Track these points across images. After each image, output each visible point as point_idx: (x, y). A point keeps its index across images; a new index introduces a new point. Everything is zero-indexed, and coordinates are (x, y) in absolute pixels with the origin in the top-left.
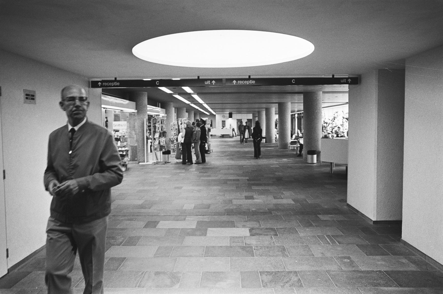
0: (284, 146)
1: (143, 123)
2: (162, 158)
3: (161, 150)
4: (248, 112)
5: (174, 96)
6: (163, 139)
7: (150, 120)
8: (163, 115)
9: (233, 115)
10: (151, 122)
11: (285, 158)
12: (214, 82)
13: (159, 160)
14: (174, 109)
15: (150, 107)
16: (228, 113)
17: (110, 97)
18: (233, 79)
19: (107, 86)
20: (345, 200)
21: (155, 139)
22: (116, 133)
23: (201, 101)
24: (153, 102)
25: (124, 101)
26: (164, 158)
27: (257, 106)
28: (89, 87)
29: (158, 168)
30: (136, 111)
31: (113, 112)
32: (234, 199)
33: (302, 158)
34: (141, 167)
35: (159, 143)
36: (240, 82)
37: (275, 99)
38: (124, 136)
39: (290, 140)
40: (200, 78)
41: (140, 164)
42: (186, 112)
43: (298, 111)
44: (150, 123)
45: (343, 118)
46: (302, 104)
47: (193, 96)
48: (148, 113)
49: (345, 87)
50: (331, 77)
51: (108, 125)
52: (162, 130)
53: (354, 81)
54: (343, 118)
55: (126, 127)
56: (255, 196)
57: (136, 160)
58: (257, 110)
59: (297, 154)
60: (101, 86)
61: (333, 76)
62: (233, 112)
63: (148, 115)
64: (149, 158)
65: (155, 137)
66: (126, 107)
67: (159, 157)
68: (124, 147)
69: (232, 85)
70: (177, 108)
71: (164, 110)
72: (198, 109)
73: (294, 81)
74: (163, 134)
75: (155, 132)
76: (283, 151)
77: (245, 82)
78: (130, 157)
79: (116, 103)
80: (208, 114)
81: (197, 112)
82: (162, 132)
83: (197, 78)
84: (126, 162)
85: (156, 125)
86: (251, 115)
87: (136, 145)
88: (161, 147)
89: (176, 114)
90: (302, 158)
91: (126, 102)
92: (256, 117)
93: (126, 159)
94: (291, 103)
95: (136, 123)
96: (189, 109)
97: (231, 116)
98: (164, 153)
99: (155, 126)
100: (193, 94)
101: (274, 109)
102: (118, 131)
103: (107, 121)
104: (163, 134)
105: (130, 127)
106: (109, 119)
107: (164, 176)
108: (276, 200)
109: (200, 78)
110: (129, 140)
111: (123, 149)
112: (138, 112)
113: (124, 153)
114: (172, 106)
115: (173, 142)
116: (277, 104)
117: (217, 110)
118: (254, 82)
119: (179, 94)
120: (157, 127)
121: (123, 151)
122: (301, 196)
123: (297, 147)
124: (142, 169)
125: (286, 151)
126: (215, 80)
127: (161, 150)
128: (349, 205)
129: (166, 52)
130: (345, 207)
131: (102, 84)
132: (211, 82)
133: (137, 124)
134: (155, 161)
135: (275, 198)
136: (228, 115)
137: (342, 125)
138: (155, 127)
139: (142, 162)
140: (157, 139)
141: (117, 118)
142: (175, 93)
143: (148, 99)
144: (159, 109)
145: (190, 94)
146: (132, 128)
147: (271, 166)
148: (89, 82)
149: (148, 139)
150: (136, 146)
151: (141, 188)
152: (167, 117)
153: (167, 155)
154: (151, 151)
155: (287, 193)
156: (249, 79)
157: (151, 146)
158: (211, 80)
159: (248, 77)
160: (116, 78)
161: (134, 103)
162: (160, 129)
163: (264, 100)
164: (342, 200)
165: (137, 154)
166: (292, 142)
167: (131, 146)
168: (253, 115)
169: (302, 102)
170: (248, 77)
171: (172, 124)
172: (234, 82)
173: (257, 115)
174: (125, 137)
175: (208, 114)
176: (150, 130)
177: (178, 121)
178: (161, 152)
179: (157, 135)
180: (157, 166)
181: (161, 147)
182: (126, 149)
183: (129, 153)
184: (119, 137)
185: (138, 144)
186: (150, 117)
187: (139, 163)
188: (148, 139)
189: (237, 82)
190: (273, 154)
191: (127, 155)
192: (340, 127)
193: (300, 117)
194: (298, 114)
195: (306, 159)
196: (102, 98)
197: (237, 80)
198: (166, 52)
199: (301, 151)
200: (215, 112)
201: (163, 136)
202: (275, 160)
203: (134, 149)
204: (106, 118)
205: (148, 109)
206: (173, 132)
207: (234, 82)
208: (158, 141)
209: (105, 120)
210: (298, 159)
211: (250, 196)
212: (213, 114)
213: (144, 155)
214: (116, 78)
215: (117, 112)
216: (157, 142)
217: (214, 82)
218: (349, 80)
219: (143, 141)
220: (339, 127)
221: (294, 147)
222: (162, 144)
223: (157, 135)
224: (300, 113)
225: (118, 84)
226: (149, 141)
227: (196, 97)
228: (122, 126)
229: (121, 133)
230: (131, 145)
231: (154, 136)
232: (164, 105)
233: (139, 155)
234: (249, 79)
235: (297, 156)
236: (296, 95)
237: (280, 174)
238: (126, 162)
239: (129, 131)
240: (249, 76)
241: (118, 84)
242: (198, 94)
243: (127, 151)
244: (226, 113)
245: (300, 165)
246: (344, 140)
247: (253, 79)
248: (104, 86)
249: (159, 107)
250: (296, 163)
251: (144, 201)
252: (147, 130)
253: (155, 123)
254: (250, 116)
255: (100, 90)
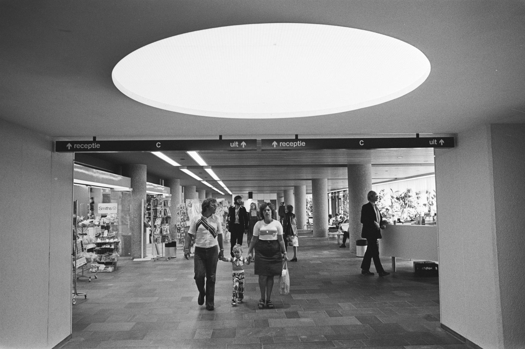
0: (321, 234)
1: (141, 206)
2: (164, 251)
3: (163, 241)
4: (272, 192)
5: (182, 170)
6: (166, 227)
7: (150, 202)
8: (167, 195)
9: (254, 195)
10: (151, 203)
11: (325, 250)
12: (243, 144)
13: (161, 255)
14: (181, 187)
15: (149, 185)
16: (248, 192)
17: (94, 170)
18: (273, 141)
19: (80, 150)
20: (437, 318)
21: (155, 226)
22: (103, 218)
23: (215, 177)
24: (154, 178)
25: (114, 177)
26: (168, 253)
27: (283, 183)
28: (53, 151)
29: (159, 267)
30: (131, 190)
31: (102, 191)
32: (271, 317)
33: (349, 250)
34: (136, 266)
35: (161, 232)
36: (284, 144)
37: (307, 174)
38: (112, 223)
39: (328, 225)
40: (223, 138)
41: (135, 260)
42: (196, 191)
43: (332, 190)
44: (149, 205)
45: (392, 197)
46: (347, 181)
47: (206, 170)
48: (147, 192)
49: (428, 154)
50: (415, 137)
51: (94, 208)
52: (165, 214)
53: (447, 143)
54: (392, 197)
55: (116, 211)
56: (300, 313)
57: (130, 256)
58: (283, 188)
59: (339, 244)
60: (72, 150)
61: (418, 135)
62: (253, 192)
63: (147, 195)
64: (147, 252)
65: (156, 224)
66: (119, 184)
67: (160, 251)
68: (113, 237)
69: (272, 148)
70: (185, 187)
71: (169, 189)
72: (211, 188)
73: (362, 143)
74: (166, 220)
75: (155, 217)
76: (319, 240)
77: (291, 144)
78: (120, 251)
79: (103, 178)
80: (223, 194)
81: (209, 191)
82: (165, 216)
83: (218, 139)
84: (114, 259)
85: (158, 208)
86: (276, 194)
87: (130, 234)
88: (164, 238)
89: (183, 194)
90: (349, 250)
91: (118, 178)
92: (281, 197)
93: (114, 255)
94: (328, 179)
95: (131, 206)
96: (200, 188)
97: (250, 196)
98: (167, 245)
99: (156, 209)
100: (207, 167)
101: (306, 188)
102: (106, 216)
103: (93, 203)
104: (166, 220)
105: (123, 211)
106: (95, 200)
107: (166, 280)
108: (334, 318)
109: (223, 138)
110: (120, 228)
111: (112, 241)
112: (133, 191)
113: (113, 247)
114: (179, 184)
115: (179, 230)
116: (311, 181)
117: (233, 189)
118: (303, 144)
119: (189, 168)
120: (158, 211)
121: (110, 244)
122: (368, 312)
123: (339, 236)
124: (137, 268)
125: (324, 240)
126: (246, 141)
127: (163, 241)
128: (443, 326)
129: (174, 77)
130: (440, 330)
131: (73, 146)
132: (239, 144)
133: (132, 207)
134: (155, 257)
135: (330, 314)
136: (247, 195)
137: (392, 206)
138: (156, 211)
139: (138, 258)
140: (158, 228)
141: (106, 199)
142: (183, 167)
143: (147, 174)
144: (162, 188)
145: (202, 167)
146: (124, 211)
147: (311, 262)
148: (53, 143)
149: (146, 226)
150: (130, 236)
151: (132, 301)
152: (172, 197)
153: (171, 248)
154: (150, 242)
155: (346, 306)
156: (297, 139)
157: (150, 235)
158: (240, 141)
159: (294, 138)
160: (94, 138)
161: (130, 179)
162: (163, 213)
163: (292, 176)
164: (429, 316)
165: (130, 246)
166: (330, 228)
167: (123, 236)
168: (278, 195)
169: (347, 177)
170: (294, 138)
171: (179, 206)
172: (275, 143)
173: (283, 195)
174: (115, 224)
175: (223, 194)
176: (149, 214)
177: (185, 202)
178: (164, 244)
179: (158, 222)
180: (158, 263)
181: (164, 238)
182: (116, 240)
183: (120, 246)
184: (105, 225)
185: (132, 233)
186: (150, 198)
187: (133, 259)
188: (146, 226)
189: (279, 144)
190: (309, 244)
191: (116, 249)
192: (389, 208)
193: (335, 197)
194: (332, 193)
195: (355, 251)
196: (75, 169)
197: (278, 141)
198: (174, 77)
199: (344, 240)
200: (231, 191)
201: (167, 223)
202: (312, 252)
203: (128, 241)
204: (92, 198)
205: (147, 187)
206: (179, 218)
207: (275, 143)
208: (159, 230)
209: (91, 201)
210: (342, 251)
211: (293, 312)
212: (229, 194)
213: (140, 248)
214: (94, 138)
215: (108, 191)
216: (158, 231)
217: (243, 144)
218: (442, 141)
219: (139, 228)
220: (387, 209)
221: (333, 235)
222: (164, 233)
223: (158, 222)
224: (335, 192)
225: (98, 146)
226: (148, 229)
227: (210, 171)
228: (110, 209)
229: (109, 220)
230: (124, 234)
231: (154, 222)
232: (168, 183)
233: (134, 248)
234: (297, 139)
235: (340, 247)
236: (341, 168)
237: (326, 273)
238: (114, 259)
239: (120, 214)
240: (297, 136)
241: (98, 146)
242: (213, 167)
243: (117, 243)
244: (244, 192)
245: (349, 259)
246: (409, 226)
247: (302, 140)
248: (76, 150)
249: (162, 185)
250: (342, 257)
251: (134, 323)
252: (145, 215)
253: (157, 206)
254: (274, 197)
255: (71, 156)
